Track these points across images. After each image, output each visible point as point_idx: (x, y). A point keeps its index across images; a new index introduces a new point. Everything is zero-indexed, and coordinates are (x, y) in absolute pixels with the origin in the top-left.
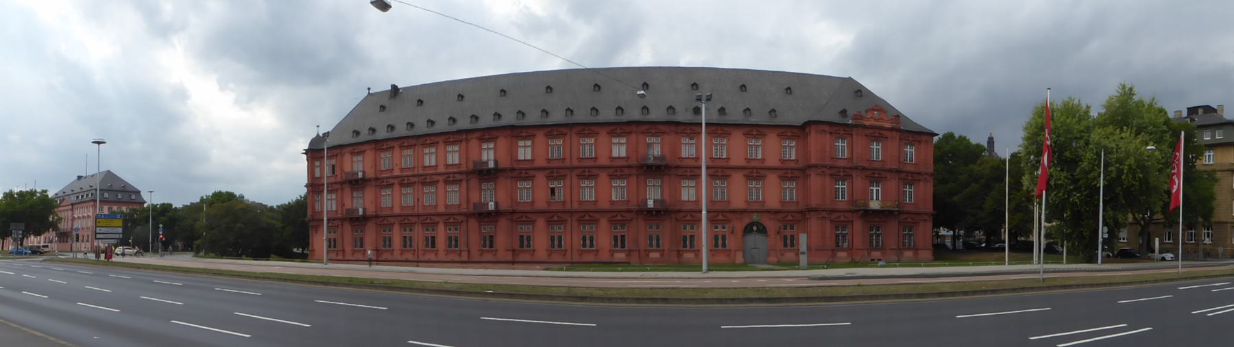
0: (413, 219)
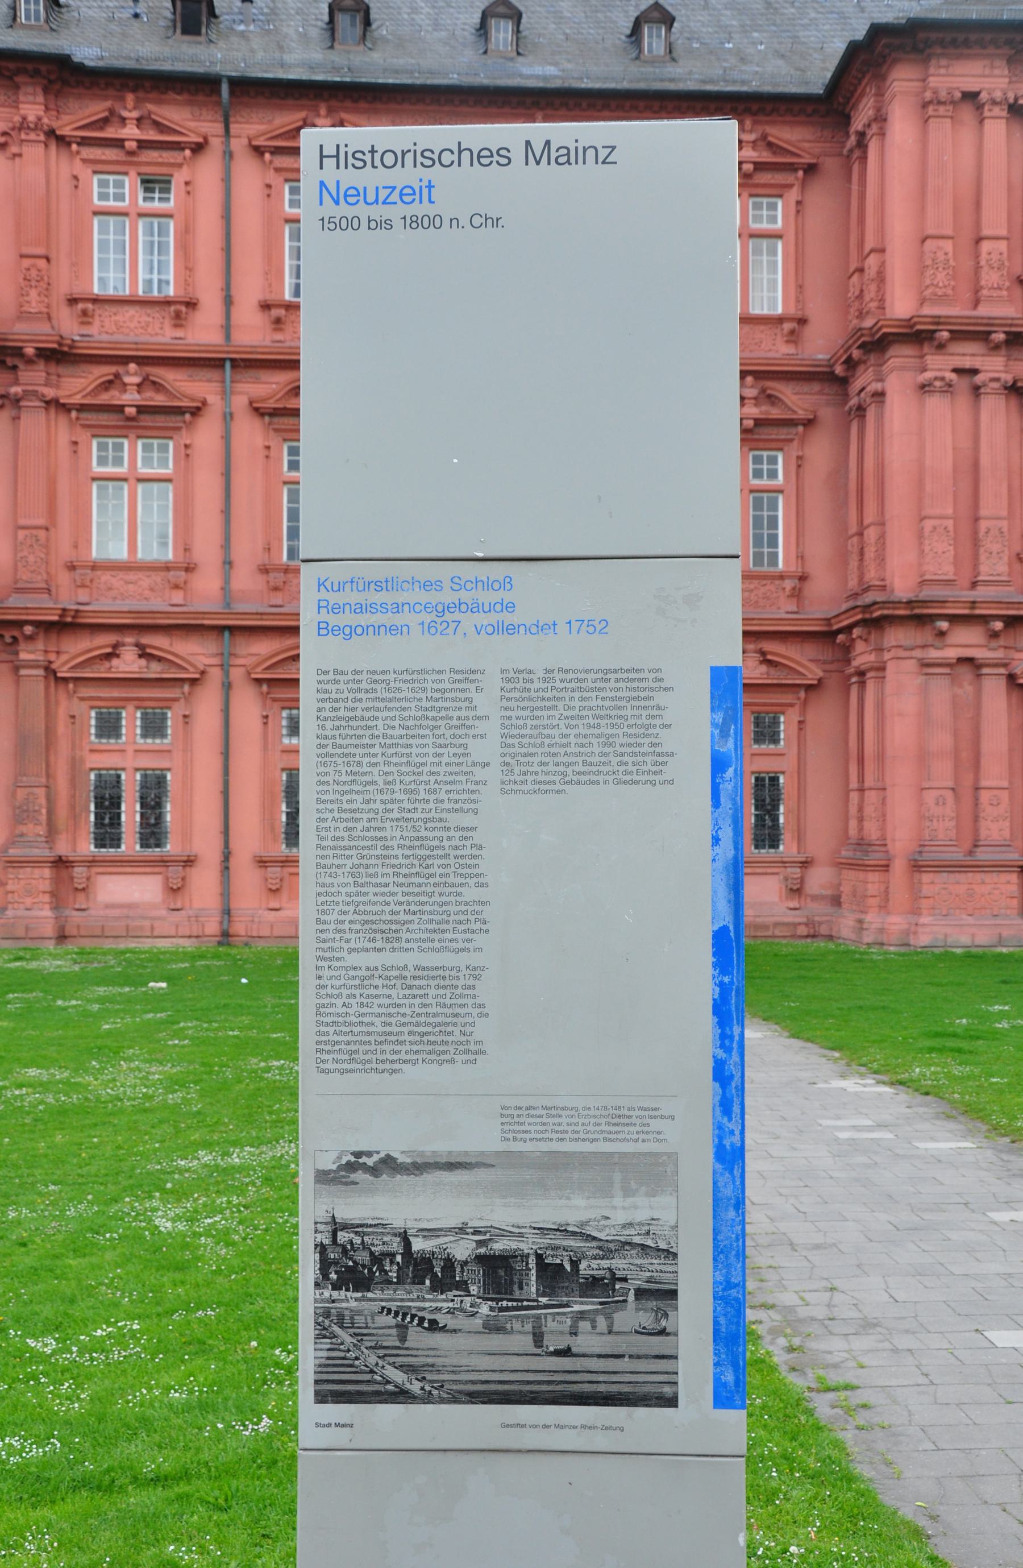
0: (196, 652)
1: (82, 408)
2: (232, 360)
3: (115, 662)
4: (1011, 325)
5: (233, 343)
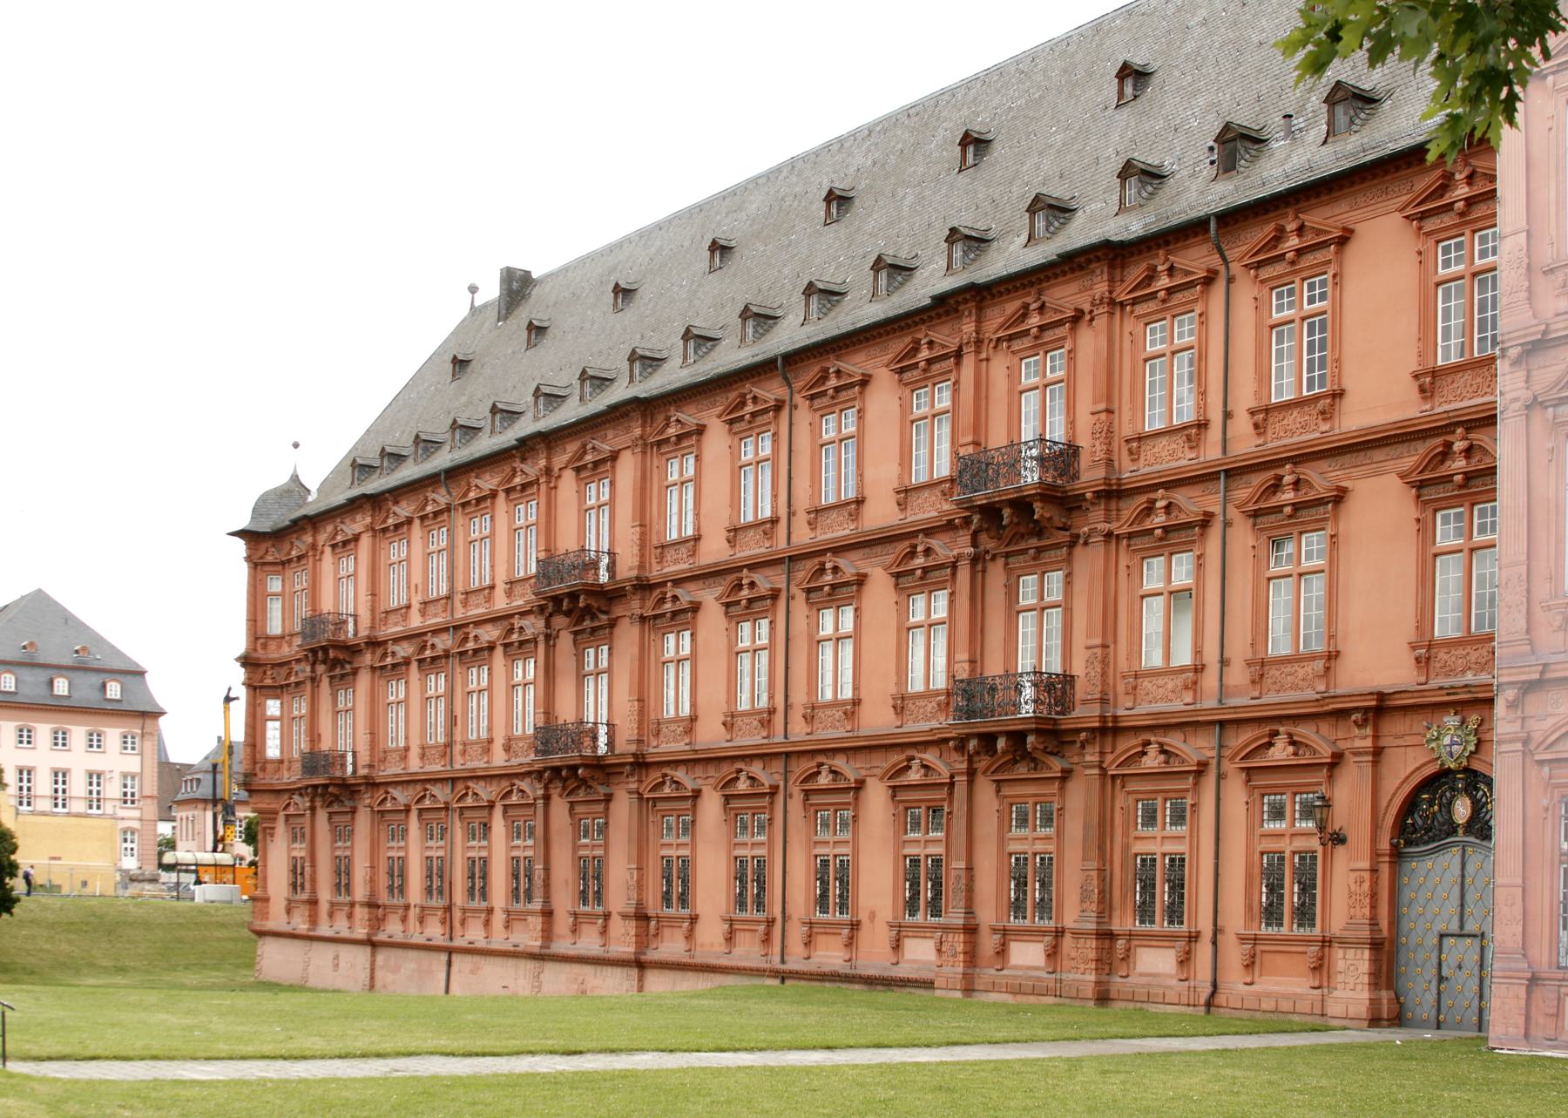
1: (1130, 536)
2: (1226, 471)
3: (1144, 759)
4: (1526, 336)
5: (56, 692)
